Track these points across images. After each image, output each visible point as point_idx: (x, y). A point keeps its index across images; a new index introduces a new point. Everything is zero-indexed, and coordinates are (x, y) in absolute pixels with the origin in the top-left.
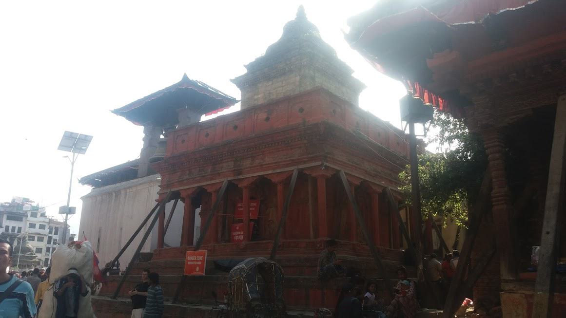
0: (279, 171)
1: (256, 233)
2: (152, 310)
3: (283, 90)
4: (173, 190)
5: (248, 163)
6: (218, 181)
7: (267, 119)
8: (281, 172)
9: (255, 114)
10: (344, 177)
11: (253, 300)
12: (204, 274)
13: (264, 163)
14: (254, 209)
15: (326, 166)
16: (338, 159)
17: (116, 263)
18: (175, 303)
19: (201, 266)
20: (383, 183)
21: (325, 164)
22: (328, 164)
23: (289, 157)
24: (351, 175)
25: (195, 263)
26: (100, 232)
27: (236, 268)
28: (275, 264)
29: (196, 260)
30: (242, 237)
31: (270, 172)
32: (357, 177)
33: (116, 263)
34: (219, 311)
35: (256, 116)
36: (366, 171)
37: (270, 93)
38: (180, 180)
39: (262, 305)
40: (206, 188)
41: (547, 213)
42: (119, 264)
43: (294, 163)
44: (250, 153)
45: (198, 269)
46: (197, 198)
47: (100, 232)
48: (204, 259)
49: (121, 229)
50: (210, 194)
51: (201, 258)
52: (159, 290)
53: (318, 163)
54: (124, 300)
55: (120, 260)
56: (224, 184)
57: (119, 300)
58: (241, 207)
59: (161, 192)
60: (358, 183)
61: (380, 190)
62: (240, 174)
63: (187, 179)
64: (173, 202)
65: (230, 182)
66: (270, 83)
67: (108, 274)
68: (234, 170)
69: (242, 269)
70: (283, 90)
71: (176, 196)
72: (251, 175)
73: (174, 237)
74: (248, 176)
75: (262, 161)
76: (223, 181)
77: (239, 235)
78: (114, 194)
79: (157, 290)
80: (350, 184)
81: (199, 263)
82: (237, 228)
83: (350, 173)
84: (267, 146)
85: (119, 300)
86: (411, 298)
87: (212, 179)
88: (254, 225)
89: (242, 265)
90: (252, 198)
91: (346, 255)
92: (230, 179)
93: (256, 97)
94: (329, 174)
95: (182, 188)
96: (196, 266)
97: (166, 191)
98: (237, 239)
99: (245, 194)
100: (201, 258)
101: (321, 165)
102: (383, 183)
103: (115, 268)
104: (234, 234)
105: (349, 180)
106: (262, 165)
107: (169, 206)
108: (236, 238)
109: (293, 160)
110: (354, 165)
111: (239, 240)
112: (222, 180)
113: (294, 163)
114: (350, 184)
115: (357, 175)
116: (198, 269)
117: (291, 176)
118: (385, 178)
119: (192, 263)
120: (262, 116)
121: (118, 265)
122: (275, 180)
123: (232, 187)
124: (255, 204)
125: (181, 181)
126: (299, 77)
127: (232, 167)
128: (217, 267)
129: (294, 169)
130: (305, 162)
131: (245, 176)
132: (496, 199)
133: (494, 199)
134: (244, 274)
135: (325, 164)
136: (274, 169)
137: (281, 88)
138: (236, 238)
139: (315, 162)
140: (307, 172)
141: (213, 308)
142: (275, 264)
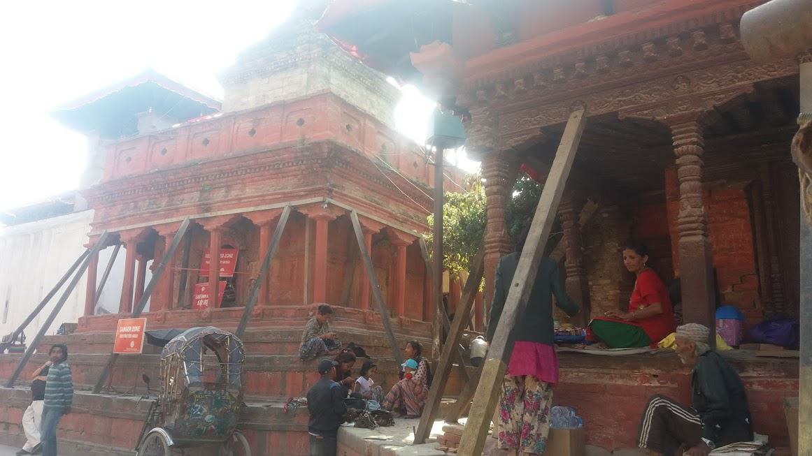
0: (263, 208)
1: (230, 295)
2: (55, 398)
3: (283, 92)
4: (110, 230)
5: (220, 195)
6: (174, 220)
7: (253, 132)
8: (266, 210)
9: (234, 124)
10: (355, 220)
11: (192, 384)
12: (141, 352)
13: (243, 196)
14: (228, 262)
15: (329, 204)
16: (349, 195)
17: (20, 336)
18: (99, 393)
19: (137, 341)
20: (416, 231)
21: (329, 200)
22: (333, 201)
23: (279, 189)
24: (367, 218)
25: (130, 336)
26: (9, 290)
27: (173, 340)
28: (230, 337)
29: (130, 331)
30: (206, 302)
31: (251, 209)
32: (377, 222)
33: (20, 336)
34: (153, 402)
35: (236, 127)
36: (391, 214)
37: (264, 96)
38: (122, 216)
39: (205, 392)
40: (157, 230)
41: (300, 201)
42: (25, 338)
43: (286, 197)
44: (224, 180)
45: (132, 344)
46: (147, 245)
47: (9, 290)
48: (141, 330)
49: (42, 288)
50: (163, 238)
51: (137, 329)
52: (66, 367)
53: (320, 199)
54: (23, 389)
55: (25, 331)
56: (182, 225)
57: (17, 388)
58: (208, 260)
59: (93, 234)
60: (377, 229)
61: (410, 241)
62: (208, 210)
63: (130, 216)
64: (111, 249)
65: (192, 221)
66: (266, 80)
67: (6, 351)
68: (200, 205)
69: (180, 342)
70: (283, 92)
71: (114, 240)
72: (224, 213)
73: (111, 299)
74: (219, 213)
75: (241, 193)
76: (182, 220)
77: (203, 300)
78: (32, 237)
79: (63, 368)
80: (365, 231)
81: (135, 336)
82: (203, 289)
83: (366, 215)
84: (248, 171)
85: (17, 388)
86: (419, 383)
87: (166, 217)
88: (227, 285)
89: (181, 337)
90: (226, 247)
91: (351, 328)
92: (192, 217)
93: (244, 100)
94: (335, 215)
95: (122, 228)
96: (130, 340)
97: (98, 233)
98: (201, 304)
99: (215, 242)
100: (137, 329)
101: (323, 202)
102: (416, 231)
103: (17, 343)
104: (198, 297)
105: (364, 224)
106: (240, 199)
107: (105, 255)
108: (200, 303)
109: (284, 193)
110: (374, 204)
111: (204, 307)
112: (181, 218)
113: (286, 197)
114: (365, 231)
115: (376, 218)
116: (132, 344)
117: (277, 218)
118: (418, 225)
119: (126, 336)
120: (247, 125)
121: (23, 338)
122: (258, 221)
123: (196, 231)
124: (231, 256)
125: (121, 218)
126: (306, 74)
127: (197, 199)
128: (156, 342)
129: (285, 207)
130: (301, 197)
131: (214, 214)
132: (489, 245)
133: (486, 246)
134: (182, 349)
135: (329, 200)
136: (257, 205)
137: (281, 89)
138: (200, 303)
139: (315, 197)
140: (304, 212)
141: (143, 398)
142: (230, 337)
